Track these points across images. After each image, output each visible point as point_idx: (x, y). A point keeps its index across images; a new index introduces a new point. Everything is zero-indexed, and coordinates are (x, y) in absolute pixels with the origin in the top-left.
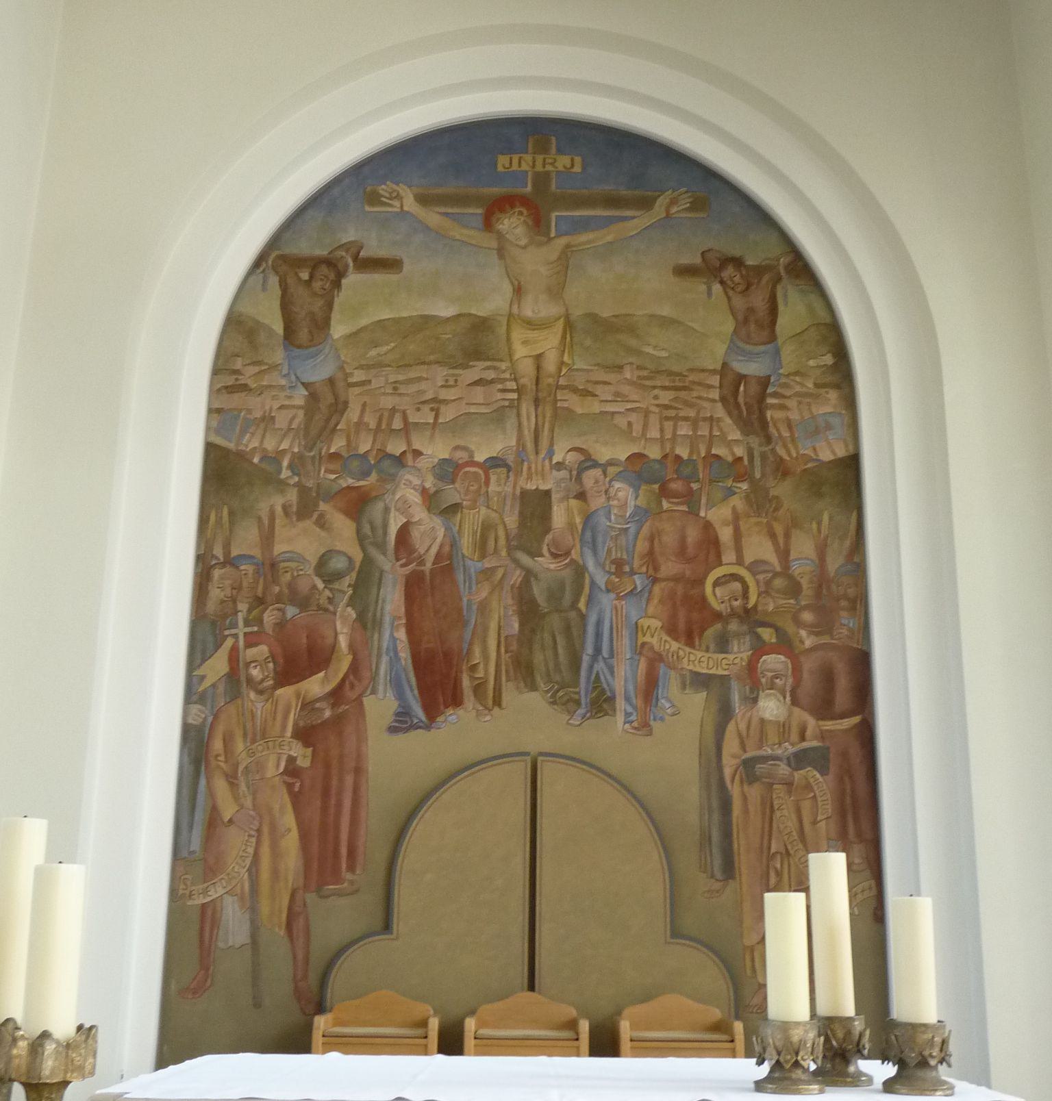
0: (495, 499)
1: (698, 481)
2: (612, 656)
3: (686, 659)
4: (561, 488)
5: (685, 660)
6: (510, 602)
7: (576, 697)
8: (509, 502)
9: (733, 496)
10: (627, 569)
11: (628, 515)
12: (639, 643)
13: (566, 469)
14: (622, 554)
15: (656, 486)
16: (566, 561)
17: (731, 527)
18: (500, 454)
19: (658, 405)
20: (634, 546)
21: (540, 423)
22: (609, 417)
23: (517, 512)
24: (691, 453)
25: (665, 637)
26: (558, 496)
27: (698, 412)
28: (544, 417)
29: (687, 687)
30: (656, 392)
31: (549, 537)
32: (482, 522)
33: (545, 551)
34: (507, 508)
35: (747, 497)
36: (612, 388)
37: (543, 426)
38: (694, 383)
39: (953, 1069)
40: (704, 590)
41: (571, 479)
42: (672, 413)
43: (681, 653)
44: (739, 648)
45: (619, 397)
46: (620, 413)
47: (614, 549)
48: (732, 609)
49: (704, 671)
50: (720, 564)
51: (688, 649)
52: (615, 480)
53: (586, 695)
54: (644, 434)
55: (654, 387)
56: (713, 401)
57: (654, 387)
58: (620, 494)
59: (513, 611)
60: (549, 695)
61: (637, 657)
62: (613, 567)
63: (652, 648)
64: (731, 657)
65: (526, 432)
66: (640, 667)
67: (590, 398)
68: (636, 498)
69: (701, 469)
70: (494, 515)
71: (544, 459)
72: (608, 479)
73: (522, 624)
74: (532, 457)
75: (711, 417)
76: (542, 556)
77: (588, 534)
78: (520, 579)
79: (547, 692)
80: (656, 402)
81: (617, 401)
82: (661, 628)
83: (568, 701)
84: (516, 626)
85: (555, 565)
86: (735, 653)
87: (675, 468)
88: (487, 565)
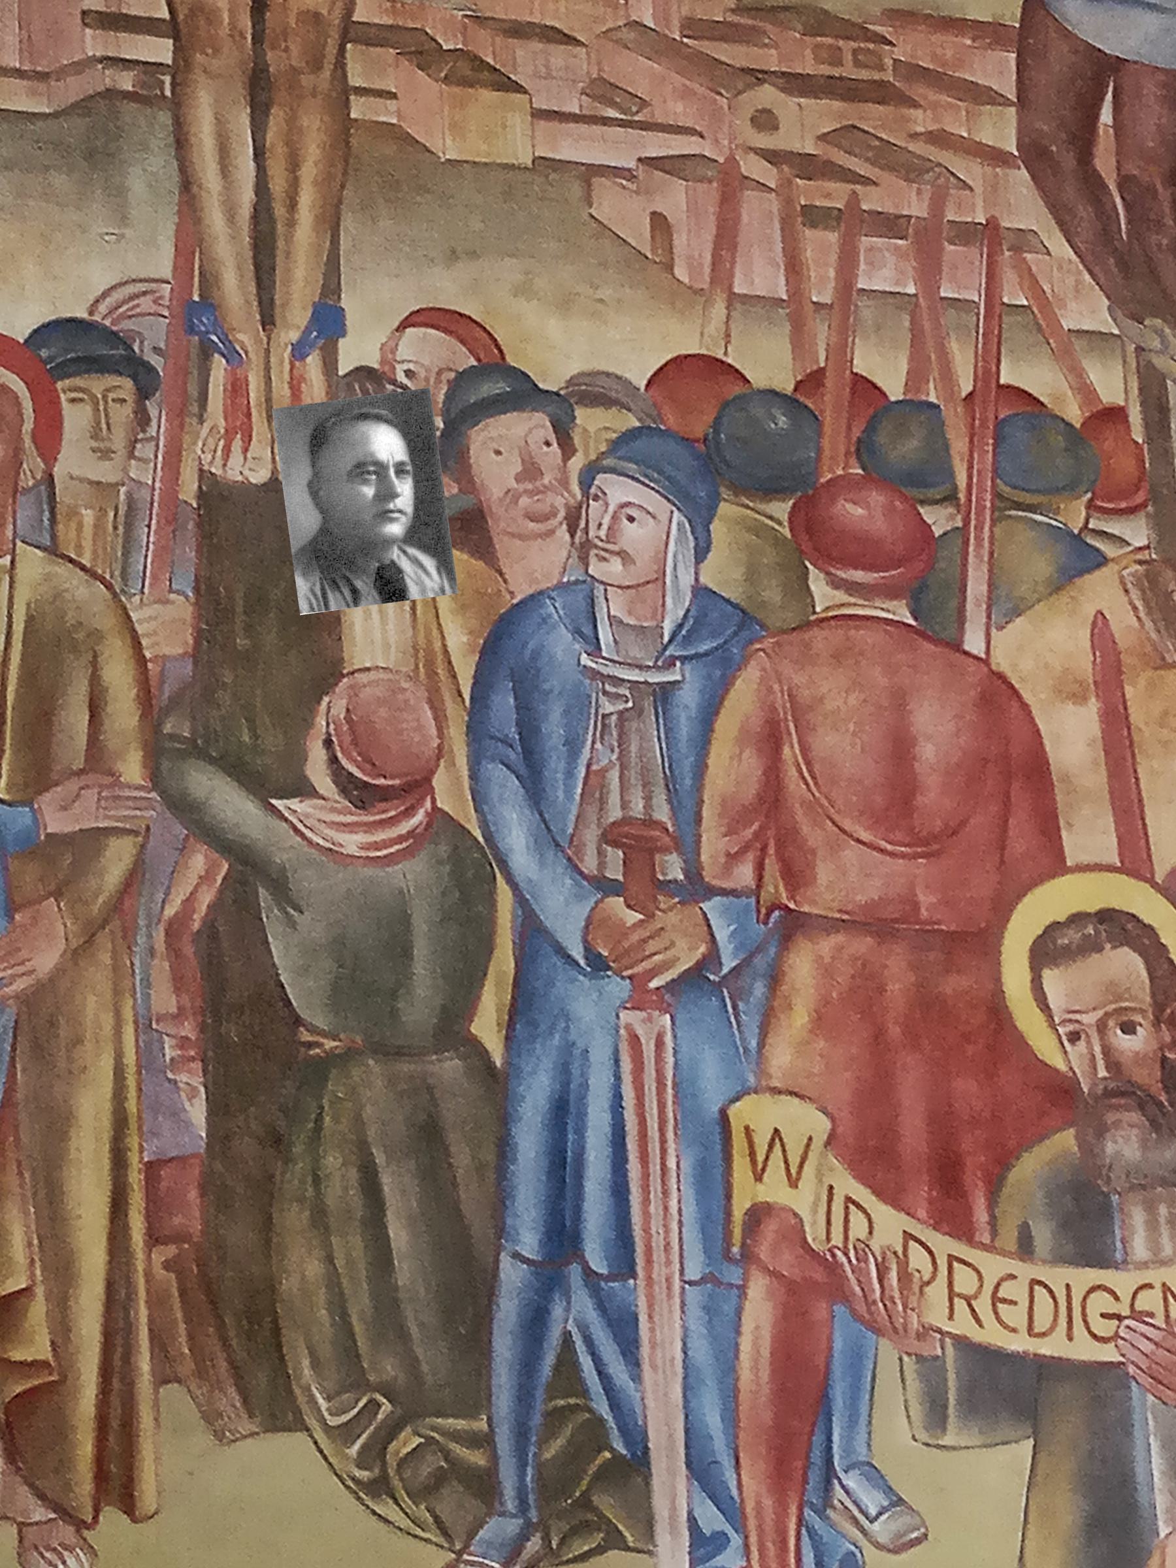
0: (88, 516)
1: (951, 498)
2: (624, 1265)
3: (939, 1288)
5: (937, 1292)
6: (165, 1000)
7: (477, 1458)
8: (147, 536)
9: (1097, 574)
10: (673, 868)
11: (668, 627)
12: (738, 1214)
14: (648, 799)
15: (781, 509)
16: (404, 827)
17: (1093, 706)
18: (103, 308)
19: (772, 157)
20: (700, 769)
21: (278, 185)
22: (576, 190)
23: (184, 582)
24: (916, 378)
25: (848, 1185)
27: (938, 204)
28: (294, 165)
29: (952, 1419)
30: (767, 95)
32: (30, 620)
33: (317, 772)
34: (144, 559)
36: (580, 62)
37: (292, 205)
38: (915, 72)
40: (998, 980)
42: (834, 196)
43: (918, 1259)
44: (1155, 1246)
45: (612, 104)
46: (617, 171)
47: (614, 776)
48: (1114, 1065)
49: (1018, 1344)
50: (1057, 866)
51: (944, 1245)
52: (606, 470)
53: (521, 1434)
55: (758, 76)
56: (997, 157)
57: (758, 76)
58: (633, 535)
59: (183, 1043)
61: (734, 1275)
62: (616, 856)
63: (795, 1233)
64: (1123, 1281)
65: (215, 219)
66: (747, 1325)
67: (488, 95)
68: (701, 553)
69: (959, 445)
70: (79, 588)
71: (299, 351)
72: (577, 463)
73: (216, 1110)
74: (246, 338)
75: (992, 225)
76: (305, 790)
77: (504, 704)
78: (206, 898)
79: (346, 1434)
80: (764, 141)
81: (606, 121)
82: (828, 1143)
83: (439, 1479)
84: (197, 1112)
85: (361, 838)
86: (1144, 1265)
87: (856, 433)
88: (56, 823)
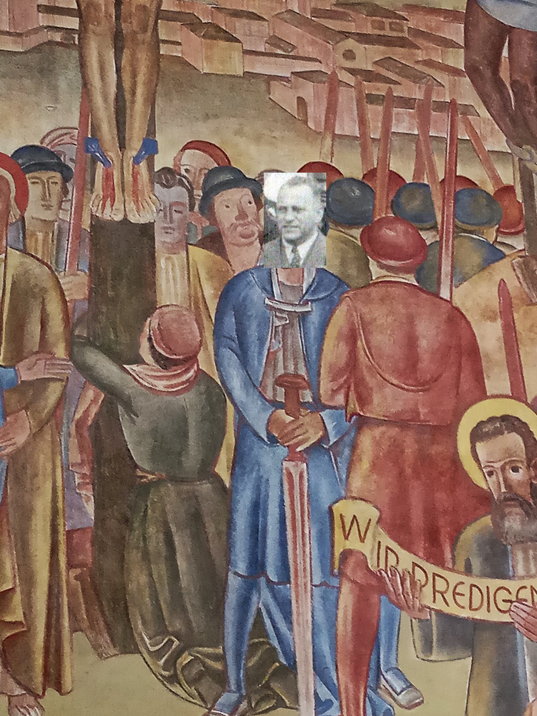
0: (40, 236)
1: (434, 227)
2: (285, 578)
4: (171, 221)
5: (428, 590)
6: (75, 457)
7: (218, 666)
8: (67, 245)
10: (307, 396)
11: (305, 286)
13: (181, 184)
14: (296, 365)
15: (357, 232)
17: (499, 322)
18: (47, 141)
19: (353, 72)
20: (320, 351)
21: (127, 84)
22: (263, 87)
23: (84, 266)
24: (418, 173)
25: (387, 541)
26: (168, 239)
27: (428, 93)
28: (134, 75)
30: (350, 43)
31: (153, 322)
32: (14, 283)
33: (145, 352)
34: (66, 255)
35: (525, 266)
36: (265, 28)
37: (134, 94)
38: (418, 33)
39: (466, 584)
40: (456, 448)
41: (192, 208)
42: (381, 89)
43: (419, 575)
44: (527, 569)
46: (281, 78)
47: (280, 354)
49: (465, 614)
50: (483, 395)
51: (431, 568)
54: (329, 124)
55: (346, 35)
56: (455, 72)
57: (346, 35)
59: (84, 476)
60: (163, 660)
61: (335, 582)
62: (281, 391)
64: (513, 585)
65: (98, 100)
66: (341, 605)
67: (223, 44)
69: (438, 203)
71: (137, 160)
73: (99, 507)
74: (113, 154)
75: (453, 103)
76: (139, 361)
77: (230, 321)
78: (94, 410)
79: (158, 655)
81: (277, 55)
82: (378, 522)
83: (201, 675)
86: (523, 578)
87: (391, 198)
88: (26, 376)
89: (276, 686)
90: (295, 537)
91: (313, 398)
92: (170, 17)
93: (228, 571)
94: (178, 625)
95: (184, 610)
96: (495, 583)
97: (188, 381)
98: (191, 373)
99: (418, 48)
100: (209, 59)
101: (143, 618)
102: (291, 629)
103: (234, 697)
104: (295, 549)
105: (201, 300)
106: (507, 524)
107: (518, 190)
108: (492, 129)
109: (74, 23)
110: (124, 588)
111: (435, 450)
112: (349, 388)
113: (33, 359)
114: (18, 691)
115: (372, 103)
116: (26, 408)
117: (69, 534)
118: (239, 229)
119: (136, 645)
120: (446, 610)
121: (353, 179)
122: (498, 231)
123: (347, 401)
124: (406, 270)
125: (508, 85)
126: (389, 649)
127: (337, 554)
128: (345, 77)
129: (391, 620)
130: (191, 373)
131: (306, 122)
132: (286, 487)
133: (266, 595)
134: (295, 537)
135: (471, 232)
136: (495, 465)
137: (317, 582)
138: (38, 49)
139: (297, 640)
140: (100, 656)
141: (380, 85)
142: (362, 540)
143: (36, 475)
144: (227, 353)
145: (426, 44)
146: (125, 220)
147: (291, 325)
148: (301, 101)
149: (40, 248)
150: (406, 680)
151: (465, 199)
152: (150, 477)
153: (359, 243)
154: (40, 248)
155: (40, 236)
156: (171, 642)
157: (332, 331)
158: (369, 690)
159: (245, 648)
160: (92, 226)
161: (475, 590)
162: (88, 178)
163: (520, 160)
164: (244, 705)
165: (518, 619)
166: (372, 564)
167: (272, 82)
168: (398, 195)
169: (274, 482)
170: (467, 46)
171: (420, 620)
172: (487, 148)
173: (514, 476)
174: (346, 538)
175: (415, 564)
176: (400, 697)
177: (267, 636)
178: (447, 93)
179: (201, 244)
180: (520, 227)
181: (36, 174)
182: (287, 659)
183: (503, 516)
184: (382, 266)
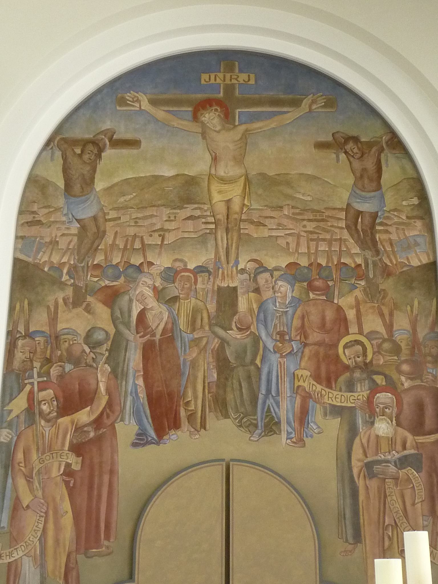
0: (201, 293)
2: (278, 394)
4: (243, 285)
5: (326, 397)
6: (211, 360)
8: (210, 295)
10: (287, 338)
13: (247, 273)
15: (305, 284)
19: (306, 232)
21: (230, 244)
23: (215, 301)
24: (328, 262)
27: (332, 236)
28: (232, 240)
30: (305, 223)
31: (236, 317)
34: (209, 299)
35: (365, 290)
37: (232, 246)
40: (338, 351)
41: (250, 280)
42: (315, 236)
43: (323, 392)
44: (361, 389)
46: (281, 236)
47: (278, 325)
49: (339, 404)
50: (348, 334)
51: (327, 390)
54: (297, 250)
55: (304, 220)
56: (342, 228)
57: (304, 220)
59: (213, 366)
62: (278, 336)
64: (356, 394)
65: (221, 250)
67: (261, 227)
71: (232, 267)
73: (218, 375)
76: (231, 329)
77: (262, 315)
78: (217, 345)
79: (236, 419)
83: (250, 425)
86: (359, 392)
87: (318, 271)
89: (274, 428)
90: (281, 382)
91: (289, 338)
92: (245, 221)
93: (259, 393)
94: (242, 410)
95: (244, 405)
96: (349, 394)
97: (248, 335)
98: (249, 332)
99: (328, 221)
100: (257, 233)
101: (231, 408)
102: (279, 410)
103: (260, 431)
104: (281, 386)
105: (252, 310)
106: (355, 375)
107: (363, 265)
108: (354, 246)
109: (213, 226)
110: (225, 399)
111: (331, 352)
112: (301, 334)
113: (198, 331)
114: (193, 430)
115: (312, 241)
116: (196, 346)
117: (209, 383)
118: (266, 286)
119: (229, 416)
120: (332, 403)
121: (305, 267)
122: (355, 279)
123: (300, 339)
124: (322, 295)
125: (360, 231)
126: (312, 416)
127: (295, 387)
128: (303, 234)
129: (313, 407)
130: (249, 332)
131: (289, 250)
132: (279, 366)
133: (272, 401)
134: (281, 382)
135: (346, 280)
136: (352, 356)
137: (288, 396)
138: (202, 235)
139: (281, 414)
140: (218, 419)
141: (315, 235)
142: (304, 382)
143: (199, 366)
144: (260, 325)
145: (332, 220)
146: (228, 286)
147: (282, 315)
148: (288, 243)
149: (201, 297)
150: (318, 426)
151: (344, 270)
152: (235, 365)
153: (306, 287)
154: (201, 297)
155: (201, 293)
156: (240, 415)
157: (296, 316)
158: (305, 429)
159: (264, 416)
160: (218, 289)
161: (343, 396)
162: (217, 274)
163: (364, 255)
164: (263, 434)
165: (357, 405)
166: (307, 390)
167: (278, 238)
168: (320, 271)
169: (275, 365)
170: (346, 219)
171: (323, 407)
172: (352, 252)
173: (358, 360)
174: (299, 381)
175: (322, 389)
176: (315, 431)
177: (271, 412)
178: (339, 235)
179: (253, 292)
180: (363, 278)
181: (201, 274)
182: (278, 419)
183: (353, 372)
184: (314, 294)
